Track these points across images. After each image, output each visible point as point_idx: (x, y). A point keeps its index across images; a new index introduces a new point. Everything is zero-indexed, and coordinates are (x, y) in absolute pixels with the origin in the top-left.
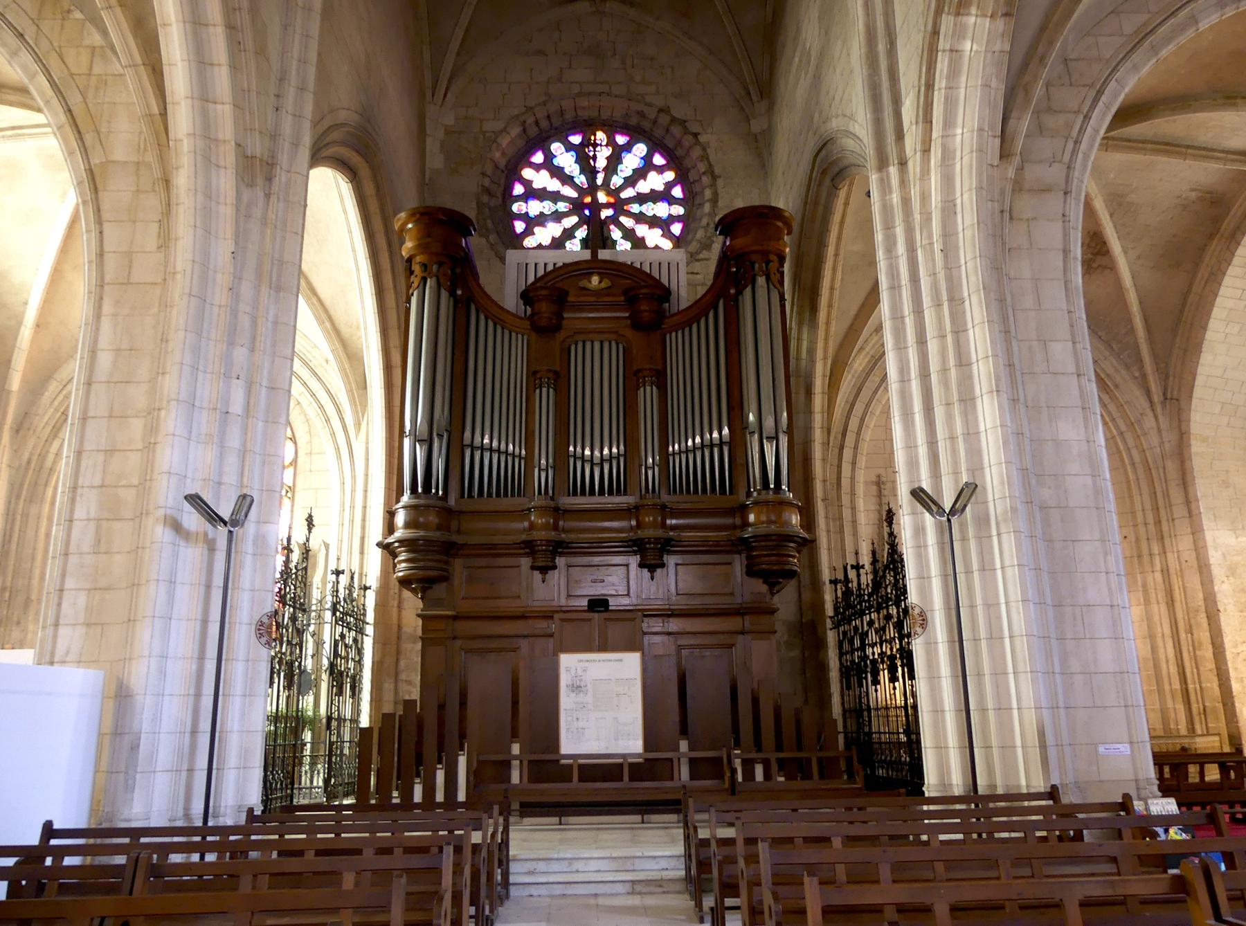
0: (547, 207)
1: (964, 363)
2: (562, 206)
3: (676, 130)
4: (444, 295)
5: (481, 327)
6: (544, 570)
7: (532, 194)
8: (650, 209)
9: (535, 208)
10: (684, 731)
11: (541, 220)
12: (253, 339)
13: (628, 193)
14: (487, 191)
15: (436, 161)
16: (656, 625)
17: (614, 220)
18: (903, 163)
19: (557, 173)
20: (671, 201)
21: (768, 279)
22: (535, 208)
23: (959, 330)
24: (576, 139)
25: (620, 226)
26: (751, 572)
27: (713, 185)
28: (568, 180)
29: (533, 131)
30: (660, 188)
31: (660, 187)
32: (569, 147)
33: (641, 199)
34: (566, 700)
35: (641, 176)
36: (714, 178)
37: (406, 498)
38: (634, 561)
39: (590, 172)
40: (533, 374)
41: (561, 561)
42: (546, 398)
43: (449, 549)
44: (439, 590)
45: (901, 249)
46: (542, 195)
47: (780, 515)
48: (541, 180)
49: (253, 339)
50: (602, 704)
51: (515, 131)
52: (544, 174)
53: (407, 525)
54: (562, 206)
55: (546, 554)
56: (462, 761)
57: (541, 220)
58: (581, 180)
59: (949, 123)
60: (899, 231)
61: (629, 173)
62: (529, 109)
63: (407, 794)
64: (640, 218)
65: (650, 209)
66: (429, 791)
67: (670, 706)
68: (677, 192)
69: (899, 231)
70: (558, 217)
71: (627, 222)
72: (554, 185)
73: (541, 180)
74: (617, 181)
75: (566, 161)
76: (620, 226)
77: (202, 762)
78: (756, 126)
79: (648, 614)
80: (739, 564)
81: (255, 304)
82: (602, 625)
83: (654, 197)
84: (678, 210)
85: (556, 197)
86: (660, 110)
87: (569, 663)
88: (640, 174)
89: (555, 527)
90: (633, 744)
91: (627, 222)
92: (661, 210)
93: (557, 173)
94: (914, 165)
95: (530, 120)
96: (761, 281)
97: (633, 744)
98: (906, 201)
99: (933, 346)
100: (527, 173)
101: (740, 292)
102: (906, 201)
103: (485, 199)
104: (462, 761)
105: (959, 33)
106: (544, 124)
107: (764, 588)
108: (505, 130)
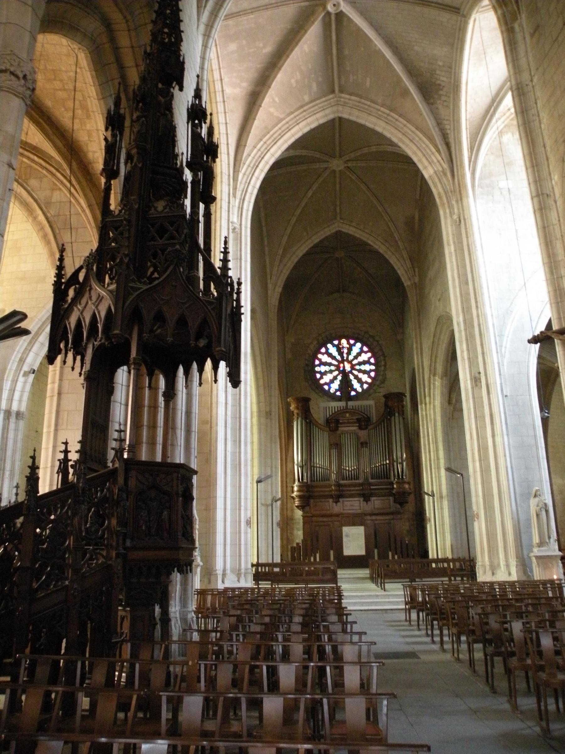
0: (327, 368)
1: (438, 459)
2: (333, 368)
3: (371, 340)
4: (304, 422)
5: (316, 430)
6: (336, 502)
7: (322, 364)
8: (363, 367)
9: (323, 369)
10: (376, 547)
11: (325, 373)
12: (271, 456)
13: (355, 362)
14: (307, 365)
15: (289, 356)
16: (369, 517)
17: (351, 372)
18: (426, 404)
19: (330, 355)
20: (371, 364)
21: (399, 414)
22: (323, 369)
23: (437, 450)
24: (336, 342)
25: (353, 374)
26: (395, 502)
27: (384, 360)
28: (334, 358)
29: (321, 341)
30: (366, 359)
31: (364, 380)
32: (334, 346)
33: (360, 364)
34: (345, 539)
35: (360, 355)
36: (385, 357)
37: (297, 483)
38: (362, 499)
39: (341, 354)
40: (330, 445)
41: (341, 500)
42: (334, 452)
43: (310, 497)
44: (307, 509)
45: (425, 427)
46: (325, 364)
47: (303, 619)
48: (325, 358)
49: (271, 456)
50: (354, 541)
51: (315, 342)
52: (326, 356)
53: (298, 491)
54: (333, 368)
55: (337, 498)
56: (318, 555)
57: (325, 373)
58: (339, 358)
59: (434, 399)
60: (425, 422)
61: (355, 354)
62: (320, 335)
63: (310, 560)
64: (360, 371)
65: (363, 367)
66: (315, 559)
67: (372, 541)
68: (372, 360)
69: (425, 422)
70: (331, 372)
71: (355, 372)
72: (329, 360)
73: (325, 358)
74: (351, 357)
75: (333, 350)
76: (353, 374)
77: (270, 553)
78: (399, 337)
79: (366, 515)
80: (391, 499)
81: (271, 447)
82: (355, 520)
83: (364, 363)
84: (373, 367)
85: (330, 364)
86: (365, 333)
87: (345, 530)
88: (359, 354)
89: (339, 490)
90: (362, 552)
91: (355, 372)
92: (367, 367)
93: (330, 355)
94: (428, 405)
95: (320, 338)
96: (397, 414)
97: (362, 552)
98: (426, 415)
99: (432, 454)
100: (320, 356)
101: (391, 417)
102: (426, 415)
103: (306, 368)
104: (318, 555)
105: (434, 380)
106: (325, 339)
107: (398, 506)
108: (312, 343)
